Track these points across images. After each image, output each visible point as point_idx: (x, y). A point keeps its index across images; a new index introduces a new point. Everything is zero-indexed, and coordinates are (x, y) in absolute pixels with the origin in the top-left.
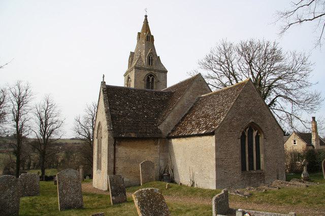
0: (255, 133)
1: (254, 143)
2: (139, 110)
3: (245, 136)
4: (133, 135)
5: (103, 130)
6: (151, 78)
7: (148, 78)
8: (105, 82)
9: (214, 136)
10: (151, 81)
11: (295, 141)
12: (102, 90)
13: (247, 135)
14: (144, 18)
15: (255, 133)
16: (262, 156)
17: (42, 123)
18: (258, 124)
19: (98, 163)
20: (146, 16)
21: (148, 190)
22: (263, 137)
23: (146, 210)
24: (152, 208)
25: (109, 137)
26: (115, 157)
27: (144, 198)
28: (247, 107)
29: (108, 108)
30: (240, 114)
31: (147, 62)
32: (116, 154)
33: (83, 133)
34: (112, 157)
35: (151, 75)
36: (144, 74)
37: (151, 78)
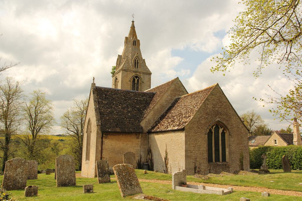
0: (221, 130)
1: (220, 138)
2: (123, 108)
3: (212, 133)
4: (118, 130)
5: (92, 126)
6: (136, 80)
7: (134, 79)
8: (95, 84)
9: (184, 131)
10: (136, 82)
11: (276, 141)
12: (92, 91)
13: (213, 132)
14: (131, 23)
15: (221, 130)
16: (227, 150)
17: (32, 118)
18: (224, 122)
19: (87, 155)
20: (133, 22)
21: (124, 165)
22: (228, 134)
23: (122, 178)
24: (126, 177)
25: (97, 132)
26: (102, 149)
27: (121, 170)
28: (214, 108)
29: (98, 106)
30: (207, 114)
31: (133, 64)
32: (103, 146)
33: (72, 129)
34: (100, 148)
35: (136, 77)
36: (131, 75)
37: (136, 80)
